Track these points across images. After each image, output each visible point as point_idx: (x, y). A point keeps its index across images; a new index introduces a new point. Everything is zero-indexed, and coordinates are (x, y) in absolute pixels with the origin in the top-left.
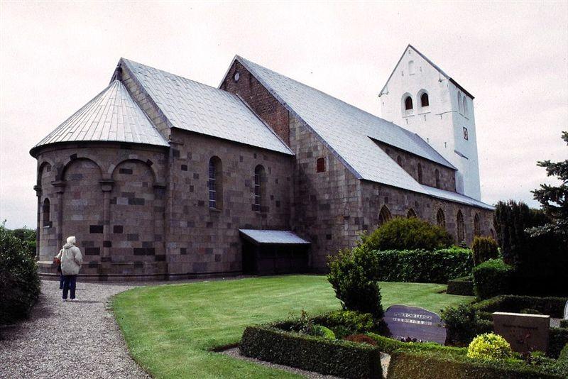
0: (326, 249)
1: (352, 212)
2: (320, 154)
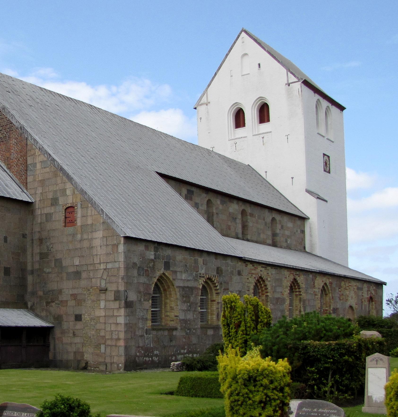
0: (74, 335)
1: (110, 282)
2: (70, 201)
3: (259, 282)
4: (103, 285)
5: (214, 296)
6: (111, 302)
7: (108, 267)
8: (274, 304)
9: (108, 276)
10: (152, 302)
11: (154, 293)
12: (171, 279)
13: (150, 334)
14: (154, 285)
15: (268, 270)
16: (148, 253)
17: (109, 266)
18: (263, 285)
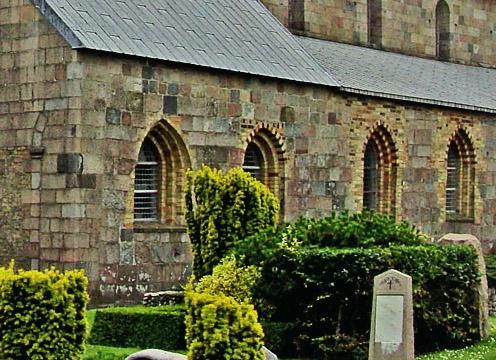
3: (380, 138)
4: (38, 142)
5: (276, 166)
6: (51, 177)
7: (47, 109)
8: (410, 182)
9: (46, 125)
10: (137, 177)
11: (140, 159)
12: (179, 132)
13: (130, 240)
14: (140, 143)
15: (399, 112)
16: (129, 80)
17: (50, 106)
18: (386, 144)
